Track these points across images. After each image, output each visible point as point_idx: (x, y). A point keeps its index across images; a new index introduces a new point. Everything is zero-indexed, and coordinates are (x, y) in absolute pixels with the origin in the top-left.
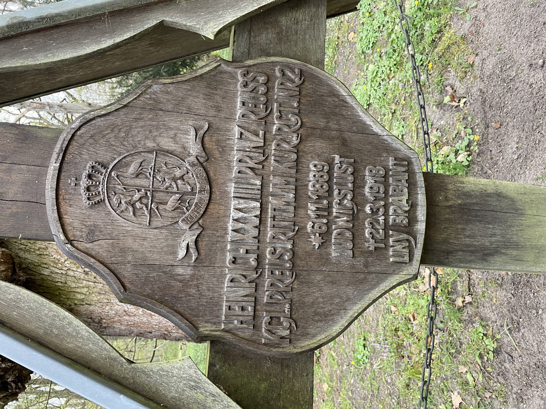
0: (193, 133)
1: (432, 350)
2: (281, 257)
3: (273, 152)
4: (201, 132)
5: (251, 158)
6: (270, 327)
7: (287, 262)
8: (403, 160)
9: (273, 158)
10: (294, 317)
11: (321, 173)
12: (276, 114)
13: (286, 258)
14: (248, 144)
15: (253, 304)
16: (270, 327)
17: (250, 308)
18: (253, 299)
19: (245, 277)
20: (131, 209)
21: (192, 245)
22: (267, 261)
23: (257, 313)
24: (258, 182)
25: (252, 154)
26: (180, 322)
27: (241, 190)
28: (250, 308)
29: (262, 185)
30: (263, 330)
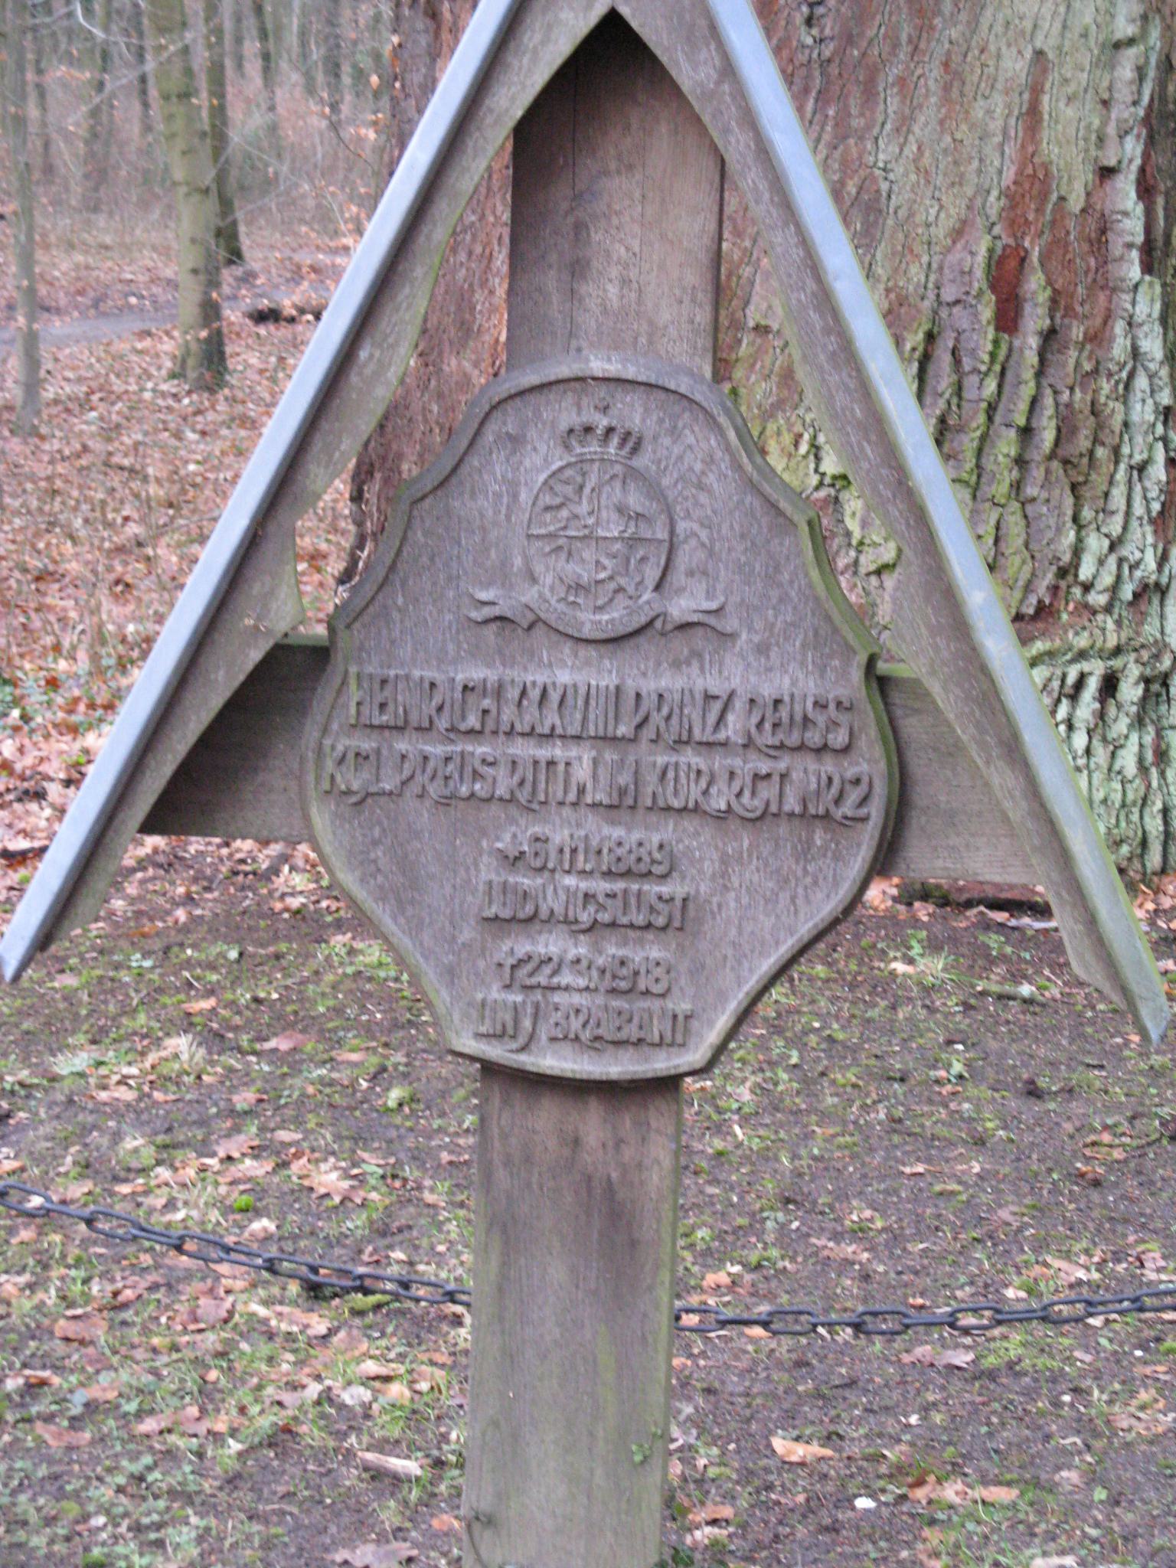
0: (714, 605)
1: (494, 712)
2: (476, 775)
3: (683, 759)
4: (712, 620)
5: (668, 718)
6: (351, 756)
7: (124, 898)
8: (687, 1031)
9: (673, 760)
10: (369, 800)
11: (646, 859)
12: (764, 767)
13: (477, 786)
14: (696, 717)
15: (392, 723)
16: (351, 756)
17: (385, 718)
18: (400, 723)
19: (440, 709)
20: (558, 501)
21: (496, 611)
22: (470, 748)
23: (376, 732)
24: (622, 730)
25: (675, 720)
26: (523, 948)
27: (602, 700)
28: (385, 718)
29: (614, 739)
30: (347, 742)
